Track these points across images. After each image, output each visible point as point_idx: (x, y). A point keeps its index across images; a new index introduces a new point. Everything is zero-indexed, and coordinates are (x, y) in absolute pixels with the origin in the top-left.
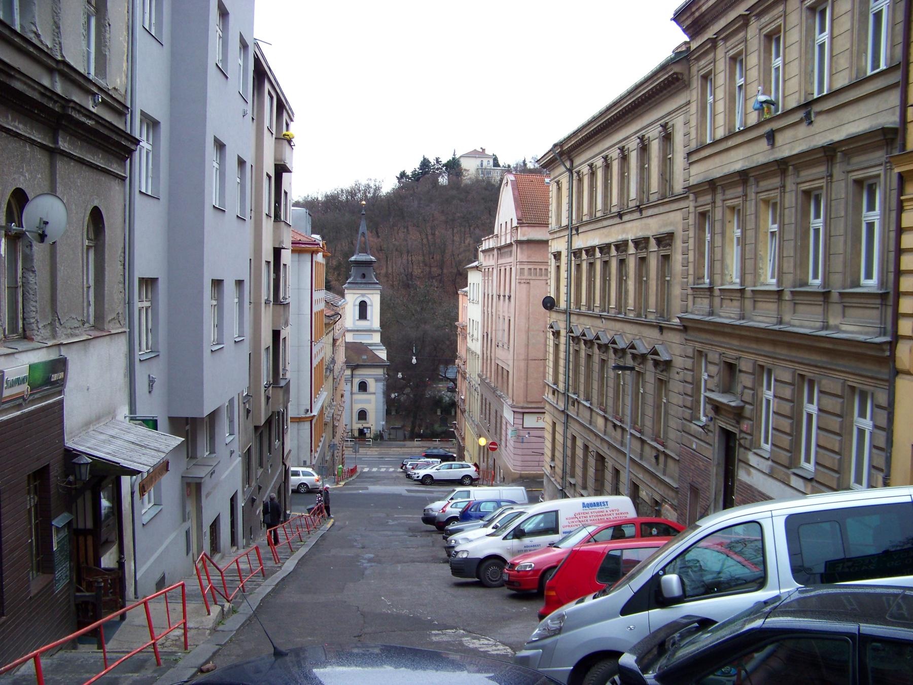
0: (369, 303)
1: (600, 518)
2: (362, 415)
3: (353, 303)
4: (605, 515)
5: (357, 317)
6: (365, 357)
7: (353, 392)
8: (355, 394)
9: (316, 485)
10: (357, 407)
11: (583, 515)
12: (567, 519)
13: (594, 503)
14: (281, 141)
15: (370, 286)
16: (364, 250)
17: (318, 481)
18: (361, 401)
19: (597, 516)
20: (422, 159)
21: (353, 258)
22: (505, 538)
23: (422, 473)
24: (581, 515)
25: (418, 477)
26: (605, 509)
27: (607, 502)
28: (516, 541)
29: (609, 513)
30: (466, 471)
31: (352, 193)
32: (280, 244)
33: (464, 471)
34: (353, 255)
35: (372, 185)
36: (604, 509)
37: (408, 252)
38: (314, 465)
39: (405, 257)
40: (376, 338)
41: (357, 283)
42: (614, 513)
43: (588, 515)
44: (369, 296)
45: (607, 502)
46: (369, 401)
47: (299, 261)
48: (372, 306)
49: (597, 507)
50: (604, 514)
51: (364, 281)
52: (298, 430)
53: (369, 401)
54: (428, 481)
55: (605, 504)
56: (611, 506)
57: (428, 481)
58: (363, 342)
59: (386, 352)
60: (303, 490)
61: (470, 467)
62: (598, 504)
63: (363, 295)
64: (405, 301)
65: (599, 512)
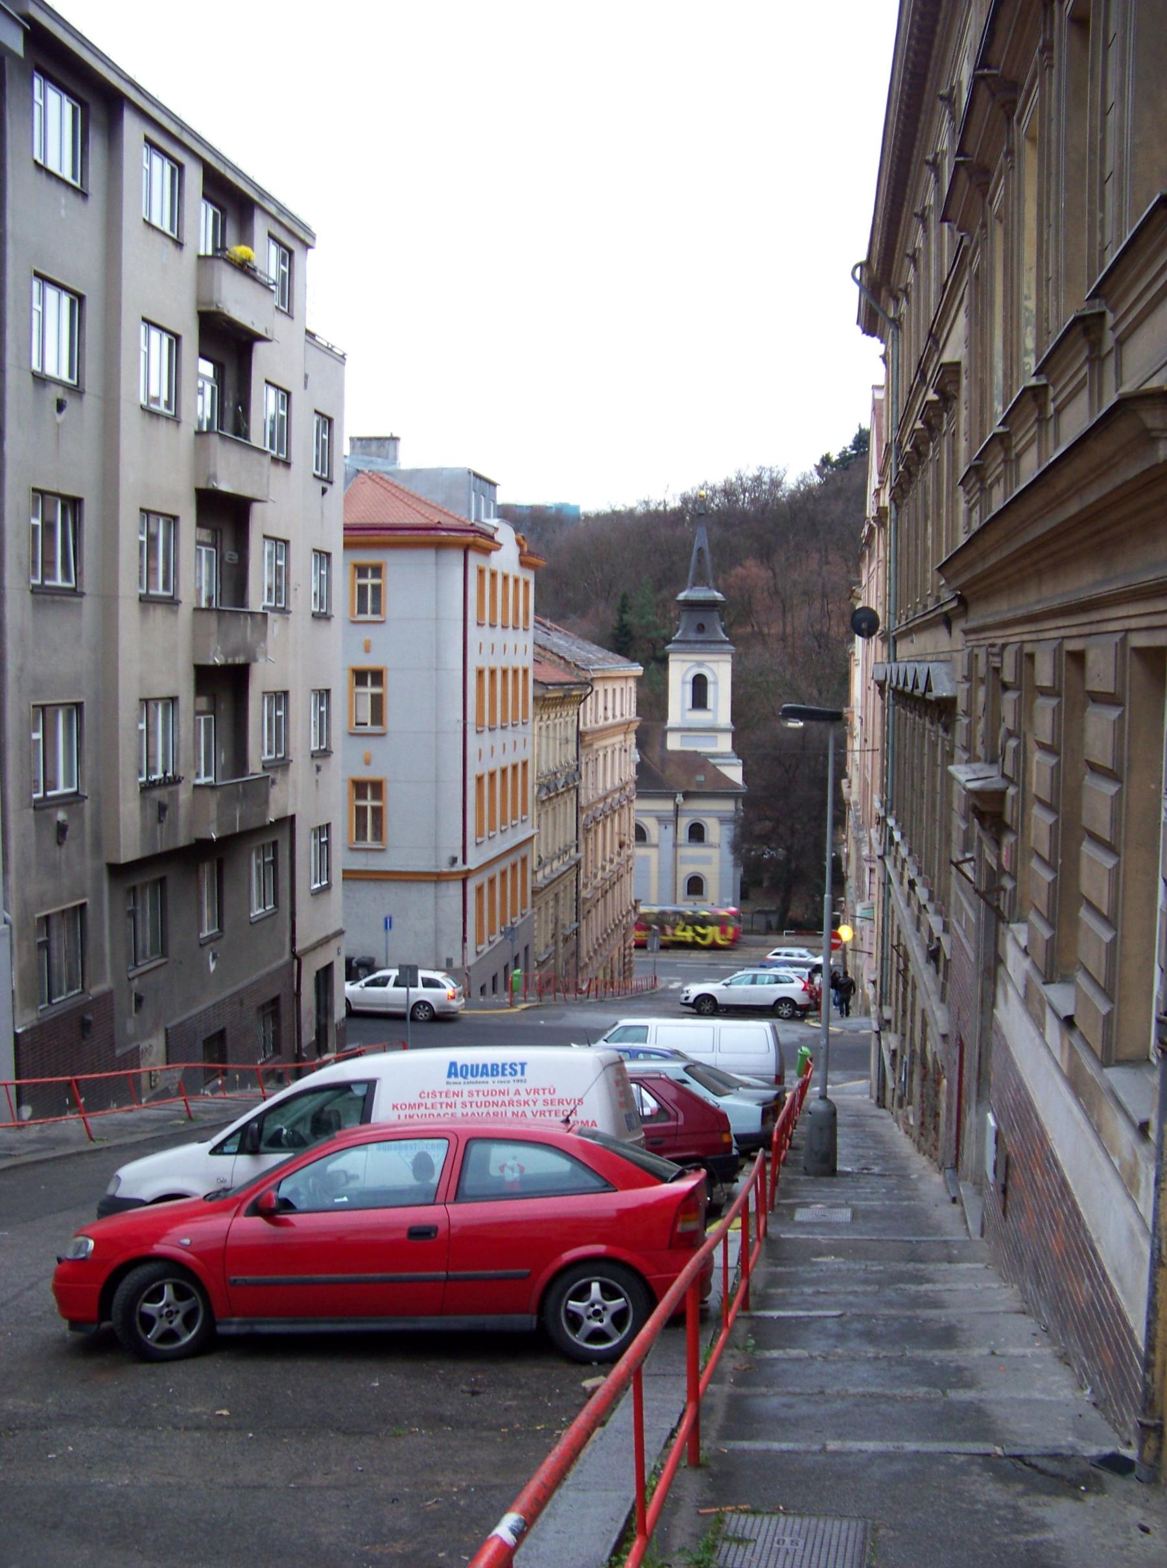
0: (710, 678)
1: (492, 1110)
2: (695, 885)
3: (680, 679)
4: (511, 1103)
5: (689, 703)
6: (701, 778)
7: (679, 842)
8: (681, 845)
9: (449, 1007)
10: (686, 871)
11: (444, 1099)
12: (395, 1107)
13: (485, 1066)
14: (209, 262)
15: (713, 647)
16: (700, 580)
17: (453, 998)
18: (694, 860)
19: (486, 1104)
20: (857, 431)
21: (682, 596)
22: (217, 1150)
23: (695, 990)
24: (438, 1099)
25: (687, 998)
26: (512, 1087)
27: (523, 1065)
28: (243, 1160)
29: (524, 1096)
30: (782, 991)
31: (728, 492)
32: (208, 480)
33: (781, 989)
34: (682, 590)
35: (766, 479)
36: (509, 1084)
37: (824, 596)
38: (469, 968)
39: (817, 604)
40: (724, 744)
41: (689, 642)
42: (541, 1098)
43: (459, 1100)
44: (712, 665)
45: (523, 1065)
46: (707, 860)
47: (437, 564)
48: (716, 683)
49: (490, 1079)
50: (506, 1099)
51: (701, 637)
52: (436, 897)
53: (707, 860)
54: (707, 1007)
55: (517, 1069)
56: (533, 1078)
57: (707, 1007)
58: (699, 749)
59: (740, 769)
60: (422, 1014)
61: (792, 982)
62: (495, 1070)
63: (700, 664)
64: (788, 677)
65: (493, 1093)
